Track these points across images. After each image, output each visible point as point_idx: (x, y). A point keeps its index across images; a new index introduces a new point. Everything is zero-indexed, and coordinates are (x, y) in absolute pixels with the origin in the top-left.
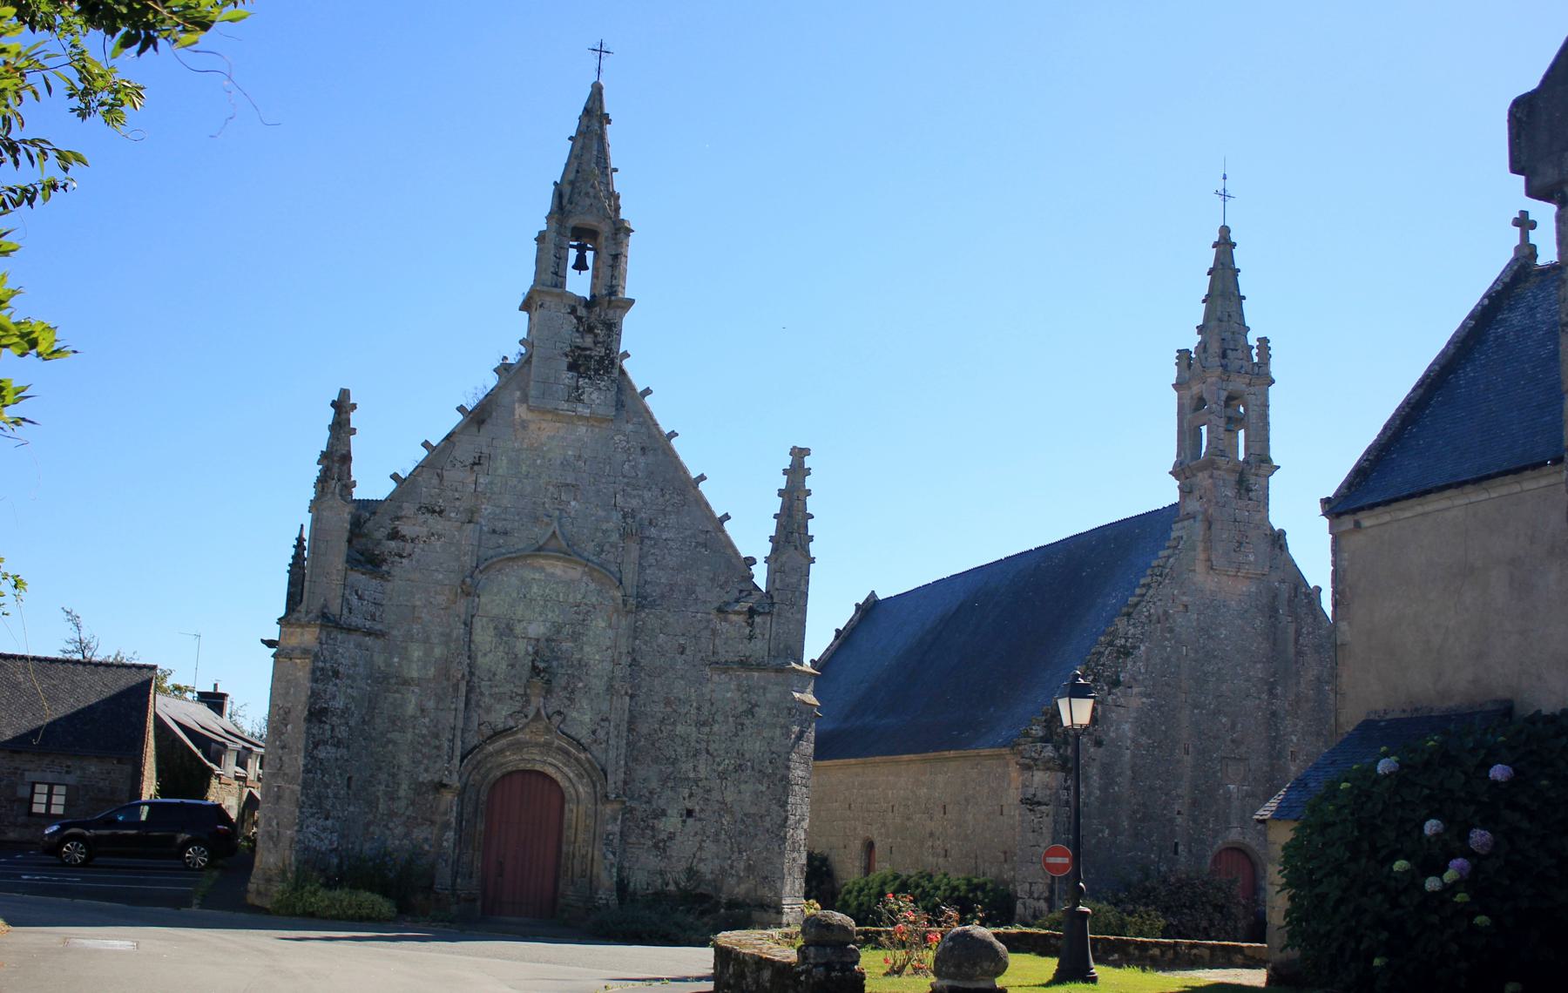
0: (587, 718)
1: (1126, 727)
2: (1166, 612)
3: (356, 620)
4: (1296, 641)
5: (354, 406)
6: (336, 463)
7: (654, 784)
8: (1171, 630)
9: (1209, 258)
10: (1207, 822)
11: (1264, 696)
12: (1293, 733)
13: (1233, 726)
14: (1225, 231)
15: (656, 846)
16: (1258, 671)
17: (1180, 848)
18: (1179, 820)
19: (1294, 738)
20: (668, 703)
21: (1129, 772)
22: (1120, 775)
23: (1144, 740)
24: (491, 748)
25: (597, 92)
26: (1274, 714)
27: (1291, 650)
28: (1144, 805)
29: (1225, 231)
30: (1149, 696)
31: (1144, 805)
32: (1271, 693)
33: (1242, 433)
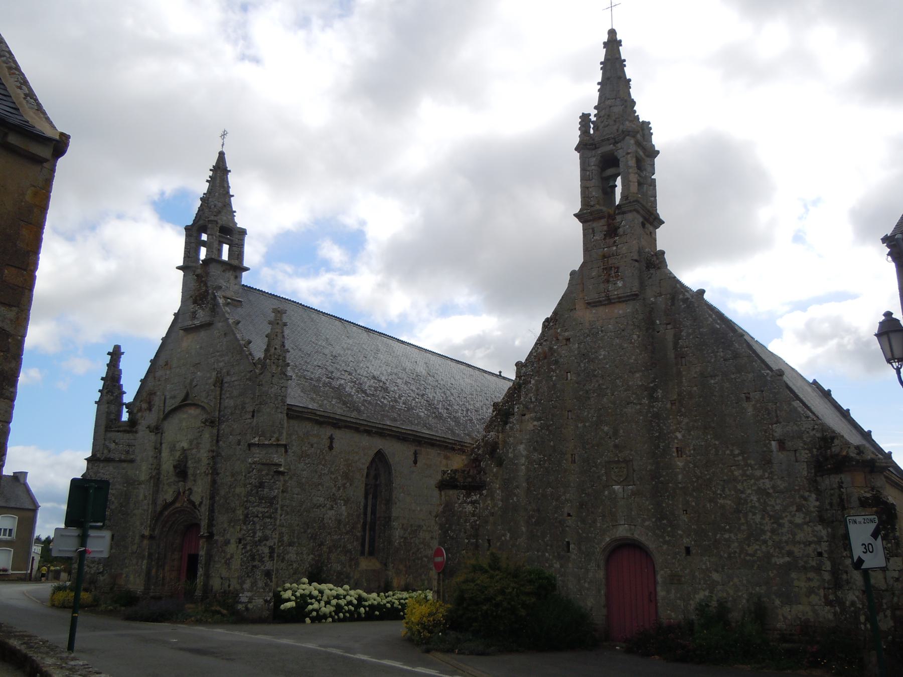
0: (200, 490)
1: (521, 447)
2: (551, 349)
3: (116, 456)
4: (676, 344)
5: (123, 353)
6: (112, 381)
7: (226, 526)
8: (556, 362)
9: (601, 54)
10: (595, 521)
11: (645, 401)
12: (677, 430)
13: (616, 433)
14: (612, 33)
15: (225, 563)
16: (637, 379)
17: (572, 546)
18: (570, 522)
19: (679, 435)
20: (233, 475)
21: (524, 485)
22: (517, 487)
23: (536, 456)
24: (166, 513)
25: (222, 155)
26: (657, 416)
27: (671, 355)
28: (538, 510)
29: (612, 33)
30: (539, 419)
31: (538, 510)
32: (651, 397)
33: (619, 181)
